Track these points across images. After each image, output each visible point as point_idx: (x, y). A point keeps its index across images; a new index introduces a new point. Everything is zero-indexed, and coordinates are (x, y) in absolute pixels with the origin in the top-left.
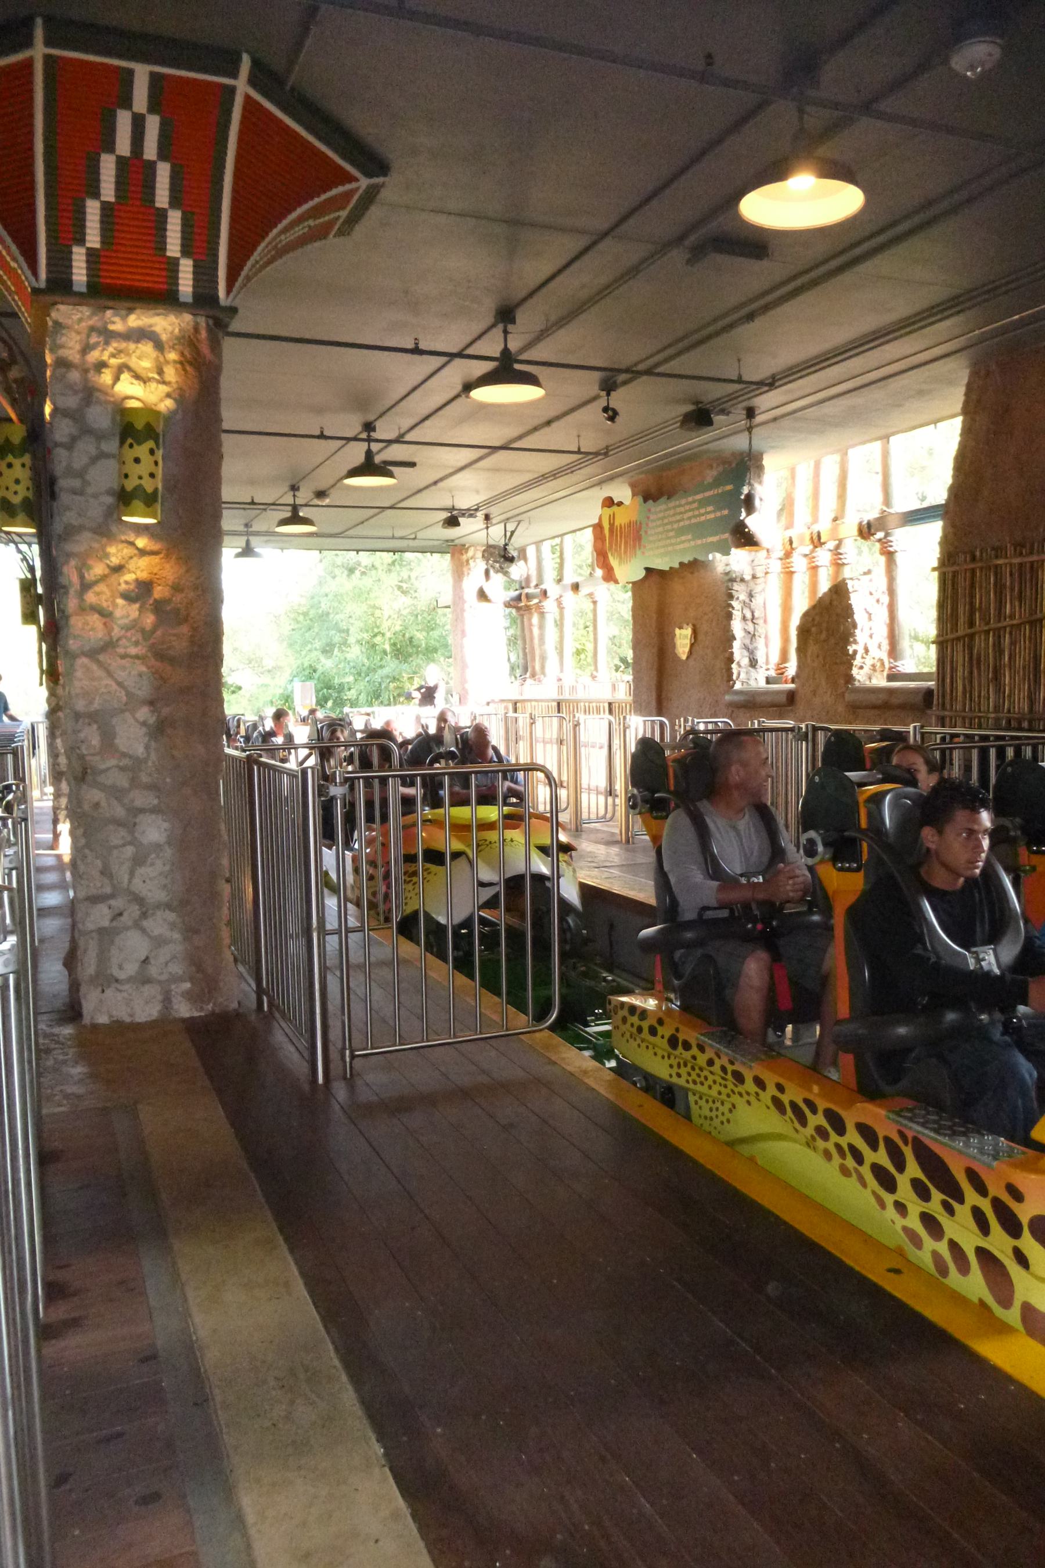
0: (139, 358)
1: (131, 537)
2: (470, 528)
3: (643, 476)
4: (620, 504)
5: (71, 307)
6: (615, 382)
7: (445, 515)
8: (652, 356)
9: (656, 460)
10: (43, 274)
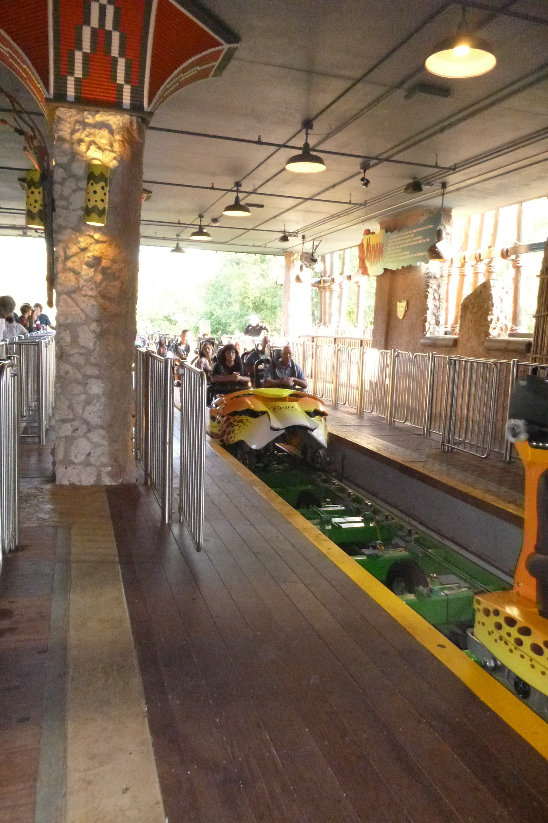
0: (101, 138)
1: (92, 233)
2: (294, 243)
3: (386, 218)
4: (373, 233)
5: (66, 109)
6: (369, 164)
7: (281, 235)
8: (387, 151)
9: (393, 210)
10: (52, 91)
